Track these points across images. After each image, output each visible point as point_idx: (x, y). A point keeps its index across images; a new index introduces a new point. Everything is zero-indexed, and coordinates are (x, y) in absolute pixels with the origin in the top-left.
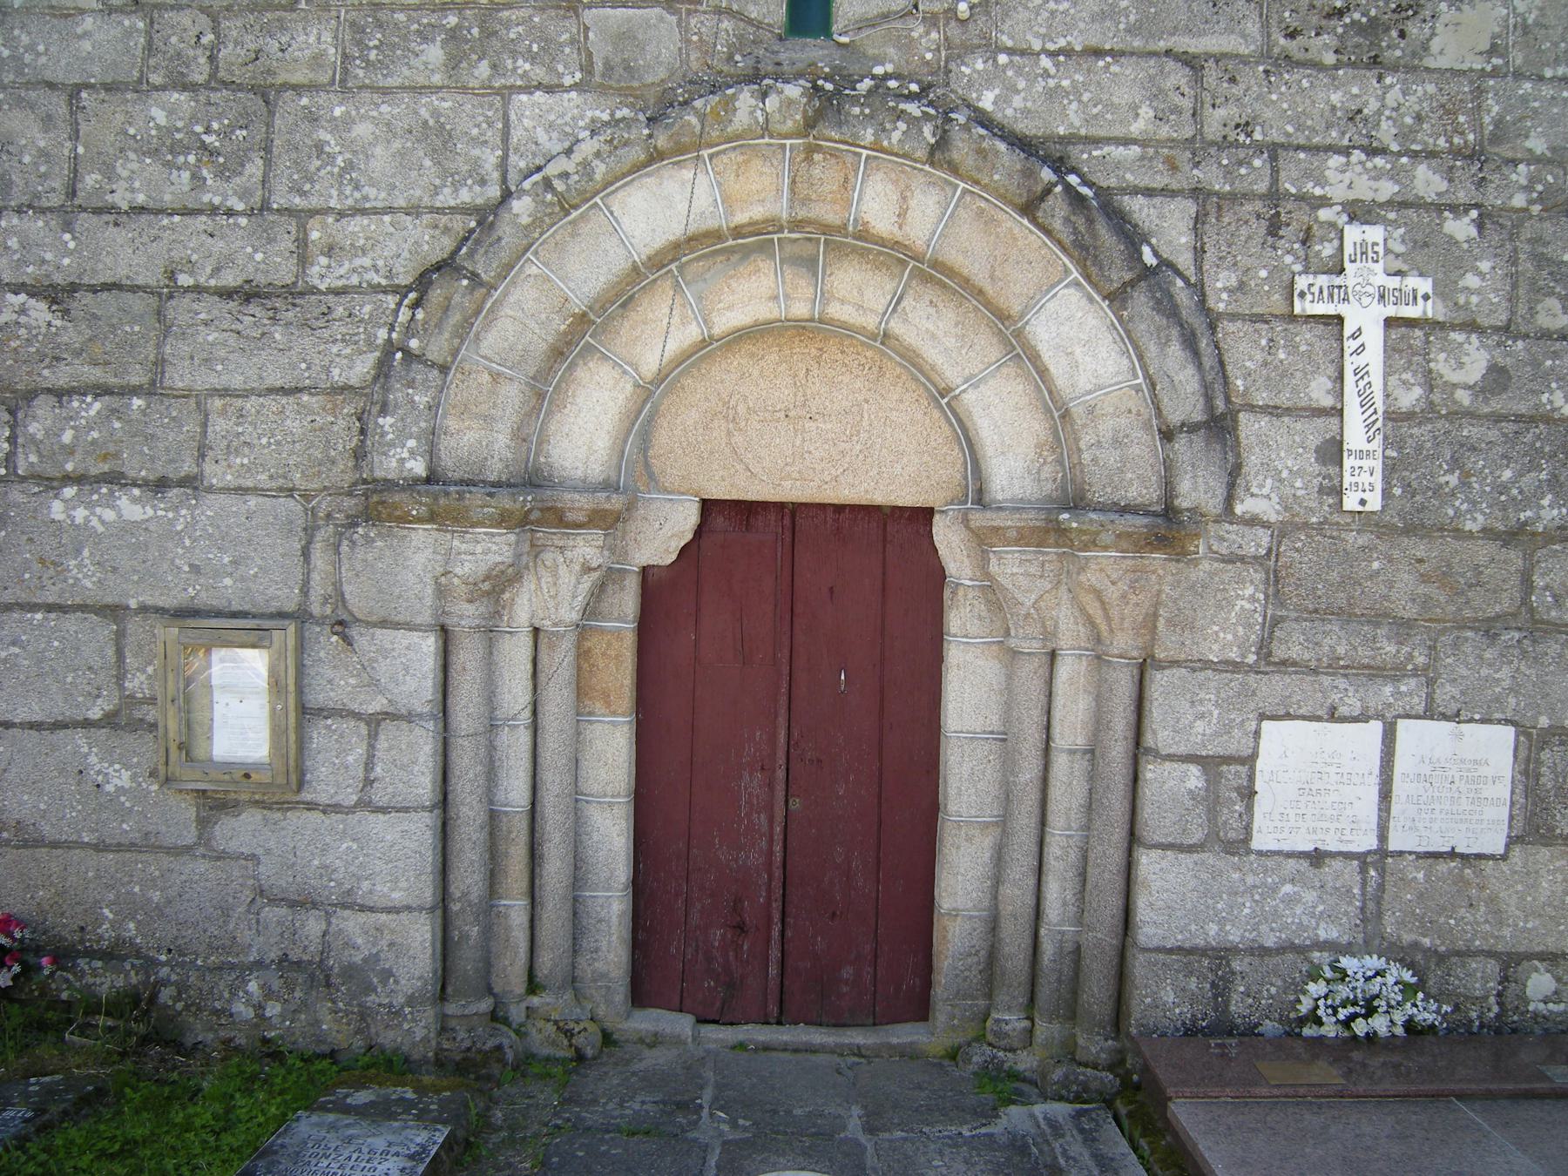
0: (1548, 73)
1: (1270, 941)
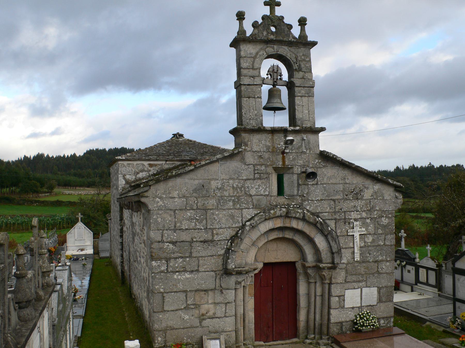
1: (348, 320)
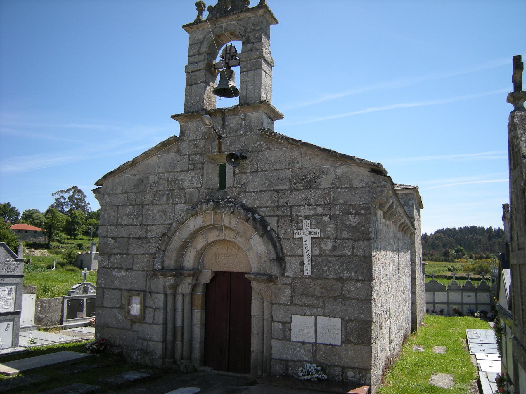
0: (343, 187)
1: (295, 359)
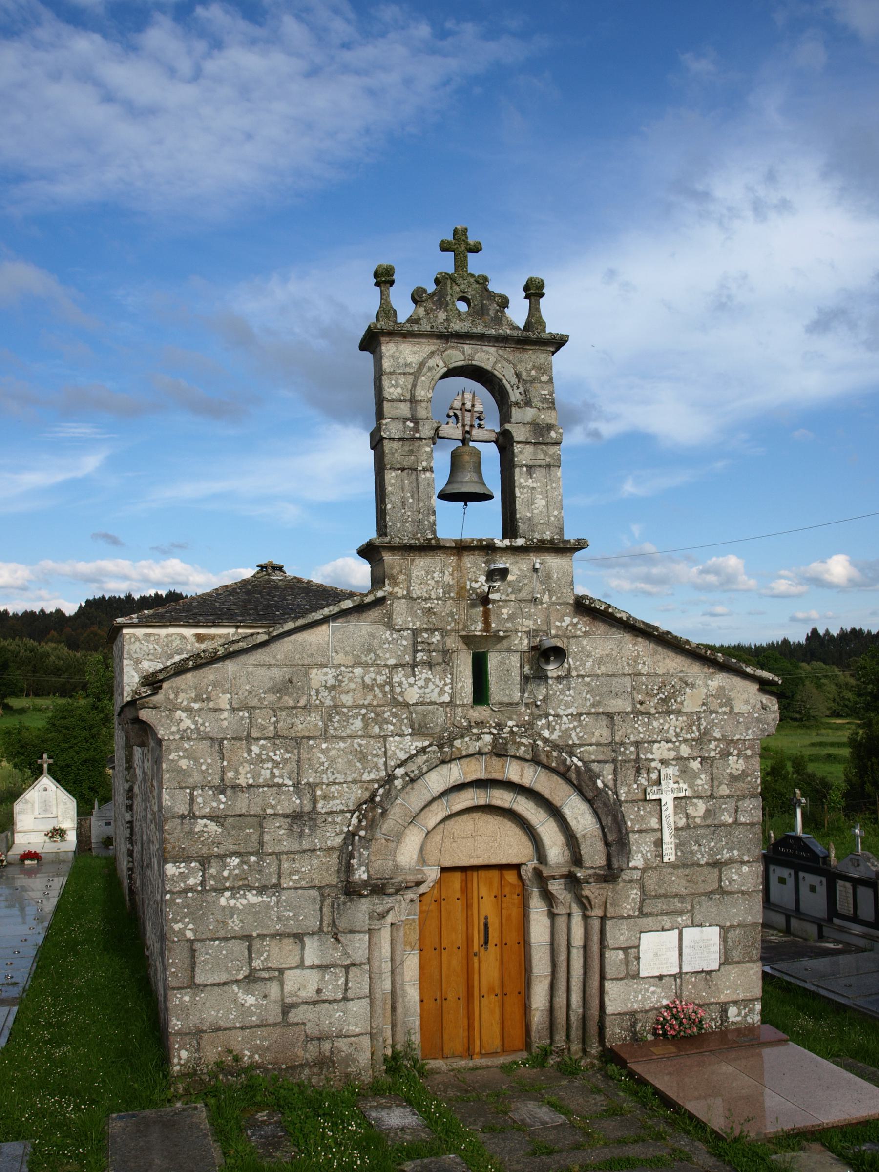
1: (647, 1008)
